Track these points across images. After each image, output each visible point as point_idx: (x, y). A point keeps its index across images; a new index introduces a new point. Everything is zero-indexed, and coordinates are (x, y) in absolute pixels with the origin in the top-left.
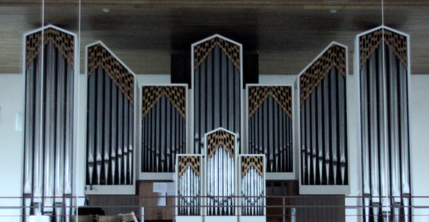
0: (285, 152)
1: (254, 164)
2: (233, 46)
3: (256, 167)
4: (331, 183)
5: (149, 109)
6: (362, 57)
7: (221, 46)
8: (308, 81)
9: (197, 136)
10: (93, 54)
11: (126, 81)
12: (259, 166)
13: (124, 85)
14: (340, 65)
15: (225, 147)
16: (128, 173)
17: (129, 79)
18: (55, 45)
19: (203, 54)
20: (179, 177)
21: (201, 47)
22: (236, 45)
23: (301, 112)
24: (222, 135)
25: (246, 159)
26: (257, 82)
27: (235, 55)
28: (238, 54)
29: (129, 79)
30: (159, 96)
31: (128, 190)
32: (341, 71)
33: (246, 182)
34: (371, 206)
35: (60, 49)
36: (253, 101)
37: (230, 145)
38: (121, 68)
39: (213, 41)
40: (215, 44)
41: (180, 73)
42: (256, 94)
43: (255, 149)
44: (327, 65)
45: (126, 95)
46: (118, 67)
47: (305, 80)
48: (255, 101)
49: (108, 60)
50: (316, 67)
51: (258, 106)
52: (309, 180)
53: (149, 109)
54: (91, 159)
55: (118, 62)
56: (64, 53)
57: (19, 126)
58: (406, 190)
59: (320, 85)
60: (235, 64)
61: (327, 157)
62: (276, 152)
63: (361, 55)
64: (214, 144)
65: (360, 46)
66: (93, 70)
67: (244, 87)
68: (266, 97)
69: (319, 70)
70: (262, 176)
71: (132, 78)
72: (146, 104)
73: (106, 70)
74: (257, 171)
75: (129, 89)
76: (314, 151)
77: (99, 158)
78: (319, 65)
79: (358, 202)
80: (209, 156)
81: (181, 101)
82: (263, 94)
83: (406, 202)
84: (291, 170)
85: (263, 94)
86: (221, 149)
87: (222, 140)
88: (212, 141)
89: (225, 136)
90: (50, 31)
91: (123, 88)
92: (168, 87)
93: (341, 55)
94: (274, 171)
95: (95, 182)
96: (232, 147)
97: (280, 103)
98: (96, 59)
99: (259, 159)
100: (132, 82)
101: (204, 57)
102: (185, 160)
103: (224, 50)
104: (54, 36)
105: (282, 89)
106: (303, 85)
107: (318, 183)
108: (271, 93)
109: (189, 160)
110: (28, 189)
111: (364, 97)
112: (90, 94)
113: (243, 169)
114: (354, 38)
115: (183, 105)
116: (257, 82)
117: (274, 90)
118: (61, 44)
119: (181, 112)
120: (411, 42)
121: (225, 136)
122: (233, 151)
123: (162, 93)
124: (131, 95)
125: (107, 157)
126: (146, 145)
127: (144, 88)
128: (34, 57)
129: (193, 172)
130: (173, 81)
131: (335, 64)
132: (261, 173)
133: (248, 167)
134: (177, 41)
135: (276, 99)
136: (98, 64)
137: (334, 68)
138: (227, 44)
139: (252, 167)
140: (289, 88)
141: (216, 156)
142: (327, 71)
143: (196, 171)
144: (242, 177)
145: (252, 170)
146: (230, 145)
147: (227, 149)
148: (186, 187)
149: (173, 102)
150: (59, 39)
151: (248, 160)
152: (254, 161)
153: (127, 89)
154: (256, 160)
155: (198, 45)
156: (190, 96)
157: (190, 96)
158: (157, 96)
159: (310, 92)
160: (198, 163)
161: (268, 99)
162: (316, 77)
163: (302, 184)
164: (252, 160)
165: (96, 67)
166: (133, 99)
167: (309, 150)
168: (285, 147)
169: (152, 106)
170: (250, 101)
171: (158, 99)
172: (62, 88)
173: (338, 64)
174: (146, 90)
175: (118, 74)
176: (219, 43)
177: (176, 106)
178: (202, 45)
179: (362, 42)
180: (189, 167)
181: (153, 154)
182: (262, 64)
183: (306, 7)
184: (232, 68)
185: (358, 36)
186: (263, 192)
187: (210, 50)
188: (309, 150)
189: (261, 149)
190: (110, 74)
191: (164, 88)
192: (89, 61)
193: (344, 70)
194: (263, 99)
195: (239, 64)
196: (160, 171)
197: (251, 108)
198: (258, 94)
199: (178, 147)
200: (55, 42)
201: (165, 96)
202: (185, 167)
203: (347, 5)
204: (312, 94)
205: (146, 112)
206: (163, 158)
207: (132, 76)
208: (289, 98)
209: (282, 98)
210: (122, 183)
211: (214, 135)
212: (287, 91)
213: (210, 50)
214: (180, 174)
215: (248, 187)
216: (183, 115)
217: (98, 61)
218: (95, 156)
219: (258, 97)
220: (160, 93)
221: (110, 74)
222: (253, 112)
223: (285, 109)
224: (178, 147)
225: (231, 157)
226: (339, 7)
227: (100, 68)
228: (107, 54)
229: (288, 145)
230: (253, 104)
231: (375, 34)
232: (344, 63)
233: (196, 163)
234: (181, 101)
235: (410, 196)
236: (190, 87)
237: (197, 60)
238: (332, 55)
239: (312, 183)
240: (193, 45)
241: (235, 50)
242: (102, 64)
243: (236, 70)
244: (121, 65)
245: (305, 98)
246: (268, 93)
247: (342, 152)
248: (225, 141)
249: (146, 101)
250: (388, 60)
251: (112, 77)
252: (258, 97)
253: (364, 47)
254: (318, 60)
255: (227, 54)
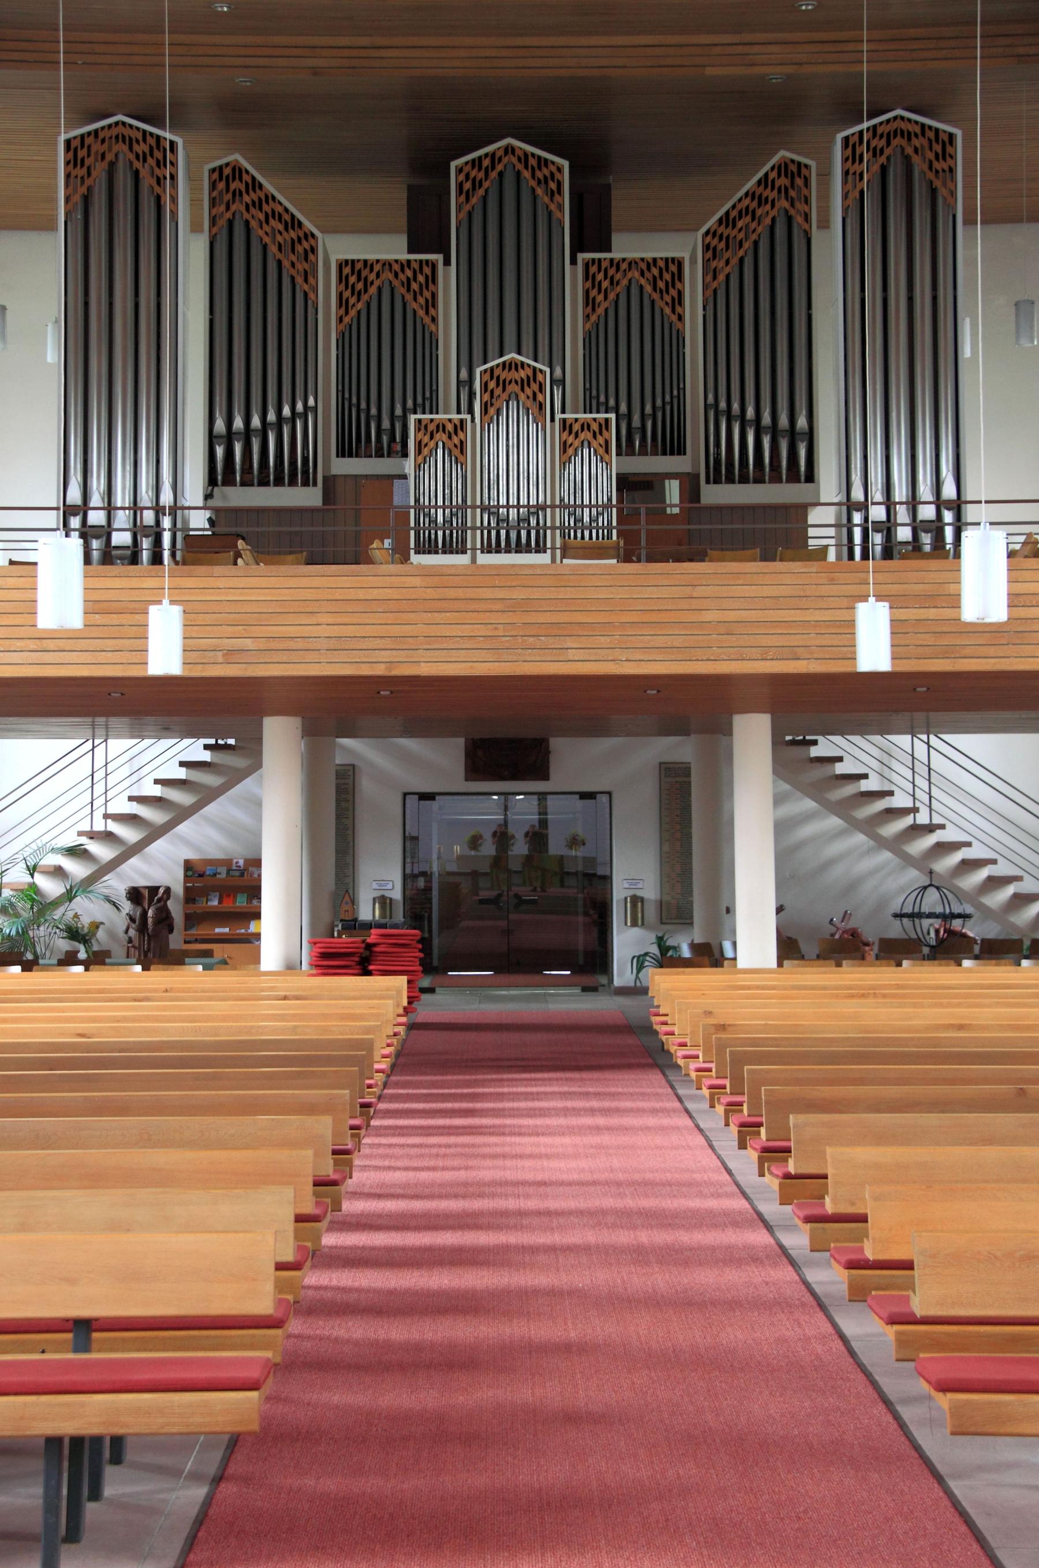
0: (668, 408)
1: (589, 435)
2: (546, 166)
3: (594, 443)
4: (776, 479)
5: (353, 313)
6: (850, 186)
7: (520, 167)
8: (722, 245)
9: (464, 374)
10: (221, 185)
11: (299, 248)
12: (601, 440)
13: (294, 258)
14: (797, 205)
15: (522, 397)
16: (305, 459)
17: (306, 245)
18: (131, 163)
19: (476, 184)
20: (418, 467)
21: (473, 167)
22: (553, 163)
23: (704, 316)
24: (517, 369)
25: (571, 426)
26: (609, 250)
27: (553, 185)
28: (559, 185)
29: (306, 245)
30: (377, 283)
31: (309, 497)
32: (799, 219)
33: (572, 477)
34: (958, 524)
35: (144, 173)
36: (593, 293)
37: (534, 394)
38: (287, 217)
39: (501, 153)
40: (505, 160)
41: (426, 231)
42: (600, 276)
43: (598, 404)
44: (769, 206)
45: (299, 280)
46: (280, 215)
47: (715, 241)
48: (599, 292)
49: (256, 200)
50: (740, 212)
51: (605, 305)
52: (722, 471)
53: (353, 313)
54: (220, 425)
55: (280, 203)
56: (154, 182)
57: (53, 354)
58: (949, 491)
59: (751, 253)
60: (553, 207)
61: (766, 419)
62: (648, 409)
63: (845, 182)
64: (498, 391)
65: (67, 163)
66: (222, 222)
67: (574, 261)
68: (625, 282)
69: (749, 218)
70: (609, 464)
71: (312, 242)
72: (347, 300)
73: (253, 224)
74: (595, 451)
75: (306, 266)
76: (736, 406)
77: (238, 423)
78: (747, 208)
79: (838, 516)
80: (487, 418)
81: (673, 292)
82: (618, 277)
83: (948, 516)
84: (681, 451)
85: (618, 277)
86: (513, 404)
87: (516, 382)
88: (492, 385)
89: (522, 374)
90: (120, 129)
91: (293, 265)
92: (396, 261)
93: (799, 182)
94: (643, 452)
95: (229, 480)
96: (540, 397)
97: (656, 296)
98: (230, 196)
99: (600, 425)
100: (313, 250)
101: (481, 192)
102: (432, 427)
103: (526, 174)
104: (131, 143)
105: (661, 264)
106: (709, 254)
107: (744, 479)
108: (637, 274)
109: (441, 427)
110: (74, 495)
111: (853, 279)
112: (217, 280)
113: (564, 446)
114: (832, 141)
115: (432, 303)
116: (609, 250)
117: (644, 266)
118: (145, 160)
119: (427, 320)
120: (184, 148)
121: (522, 374)
122: (541, 406)
123: (383, 277)
124: (311, 280)
125: (256, 422)
126: (347, 395)
127: (341, 265)
128: (83, 190)
129: (450, 455)
130: (410, 251)
131: (786, 204)
132: (606, 457)
133: (577, 443)
134: (429, 154)
135: (648, 288)
136: (233, 208)
137: (782, 212)
138: (533, 162)
139: (586, 444)
140: (680, 264)
141: (503, 419)
142: (768, 221)
143: (456, 452)
144: (563, 465)
145: (586, 451)
146: (534, 394)
147: (529, 403)
148: (433, 488)
149: (409, 297)
150: (141, 148)
151: (576, 427)
152: (589, 429)
153: (301, 266)
154: (595, 427)
155: (467, 163)
156: (448, 282)
157: (448, 282)
158: (372, 283)
159: (727, 270)
160: (461, 435)
161: (629, 288)
162: (742, 235)
163: (708, 482)
164: (586, 426)
165: (229, 215)
166: (315, 290)
167: (723, 405)
168: (668, 398)
169: (359, 306)
170: (587, 293)
171: (373, 290)
172: (149, 269)
173: (792, 205)
174: (347, 270)
175: (280, 233)
176: (514, 160)
177: (414, 305)
178: (477, 163)
179: (71, 154)
180: (440, 444)
181: (363, 416)
182: (620, 207)
183: (709, 71)
184: (546, 218)
185: (840, 137)
186: (610, 499)
187: (494, 175)
188: (723, 405)
189: (612, 402)
190: (261, 233)
191: (387, 264)
192: (213, 203)
193: (807, 218)
194: (618, 289)
195: (561, 207)
196: (380, 454)
197: (589, 309)
198: (606, 277)
199: (419, 400)
200: (132, 157)
201: (391, 282)
202: (432, 444)
203: (806, 63)
204: (732, 276)
205: (347, 320)
206: (386, 424)
207: (313, 235)
208: (678, 285)
209: (661, 285)
210: (293, 483)
211: (497, 373)
212: (673, 268)
213: (494, 175)
214: (420, 459)
215: (577, 489)
216: (433, 327)
217: (233, 203)
218: (229, 422)
219: (605, 284)
220: (378, 276)
221: (261, 233)
222: (593, 318)
223: (668, 310)
224: (419, 400)
225: (536, 421)
226: (789, 70)
227: (237, 217)
228: (255, 185)
229: (675, 393)
230: (594, 299)
231: (106, 134)
232: (807, 201)
233: (456, 434)
234: (427, 294)
235: (957, 506)
236: (447, 262)
237: (463, 198)
238: (777, 184)
239: (730, 480)
240: (454, 165)
241: (552, 174)
242: (243, 208)
243: (554, 224)
244: (286, 210)
245: (715, 284)
246: (630, 275)
247: (801, 410)
248: (523, 384)
249: (347, 294)
250: (910, 199)
251: (267, 240)
252: (605, 284)
253: (75, 166)
254: (747, 194)
255: (533, 183)
